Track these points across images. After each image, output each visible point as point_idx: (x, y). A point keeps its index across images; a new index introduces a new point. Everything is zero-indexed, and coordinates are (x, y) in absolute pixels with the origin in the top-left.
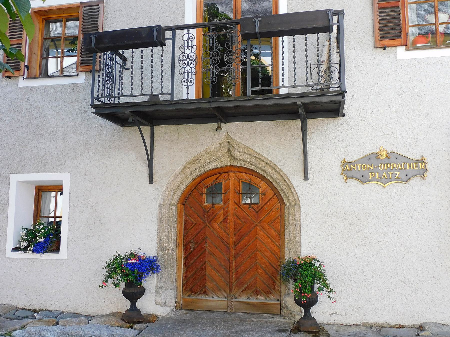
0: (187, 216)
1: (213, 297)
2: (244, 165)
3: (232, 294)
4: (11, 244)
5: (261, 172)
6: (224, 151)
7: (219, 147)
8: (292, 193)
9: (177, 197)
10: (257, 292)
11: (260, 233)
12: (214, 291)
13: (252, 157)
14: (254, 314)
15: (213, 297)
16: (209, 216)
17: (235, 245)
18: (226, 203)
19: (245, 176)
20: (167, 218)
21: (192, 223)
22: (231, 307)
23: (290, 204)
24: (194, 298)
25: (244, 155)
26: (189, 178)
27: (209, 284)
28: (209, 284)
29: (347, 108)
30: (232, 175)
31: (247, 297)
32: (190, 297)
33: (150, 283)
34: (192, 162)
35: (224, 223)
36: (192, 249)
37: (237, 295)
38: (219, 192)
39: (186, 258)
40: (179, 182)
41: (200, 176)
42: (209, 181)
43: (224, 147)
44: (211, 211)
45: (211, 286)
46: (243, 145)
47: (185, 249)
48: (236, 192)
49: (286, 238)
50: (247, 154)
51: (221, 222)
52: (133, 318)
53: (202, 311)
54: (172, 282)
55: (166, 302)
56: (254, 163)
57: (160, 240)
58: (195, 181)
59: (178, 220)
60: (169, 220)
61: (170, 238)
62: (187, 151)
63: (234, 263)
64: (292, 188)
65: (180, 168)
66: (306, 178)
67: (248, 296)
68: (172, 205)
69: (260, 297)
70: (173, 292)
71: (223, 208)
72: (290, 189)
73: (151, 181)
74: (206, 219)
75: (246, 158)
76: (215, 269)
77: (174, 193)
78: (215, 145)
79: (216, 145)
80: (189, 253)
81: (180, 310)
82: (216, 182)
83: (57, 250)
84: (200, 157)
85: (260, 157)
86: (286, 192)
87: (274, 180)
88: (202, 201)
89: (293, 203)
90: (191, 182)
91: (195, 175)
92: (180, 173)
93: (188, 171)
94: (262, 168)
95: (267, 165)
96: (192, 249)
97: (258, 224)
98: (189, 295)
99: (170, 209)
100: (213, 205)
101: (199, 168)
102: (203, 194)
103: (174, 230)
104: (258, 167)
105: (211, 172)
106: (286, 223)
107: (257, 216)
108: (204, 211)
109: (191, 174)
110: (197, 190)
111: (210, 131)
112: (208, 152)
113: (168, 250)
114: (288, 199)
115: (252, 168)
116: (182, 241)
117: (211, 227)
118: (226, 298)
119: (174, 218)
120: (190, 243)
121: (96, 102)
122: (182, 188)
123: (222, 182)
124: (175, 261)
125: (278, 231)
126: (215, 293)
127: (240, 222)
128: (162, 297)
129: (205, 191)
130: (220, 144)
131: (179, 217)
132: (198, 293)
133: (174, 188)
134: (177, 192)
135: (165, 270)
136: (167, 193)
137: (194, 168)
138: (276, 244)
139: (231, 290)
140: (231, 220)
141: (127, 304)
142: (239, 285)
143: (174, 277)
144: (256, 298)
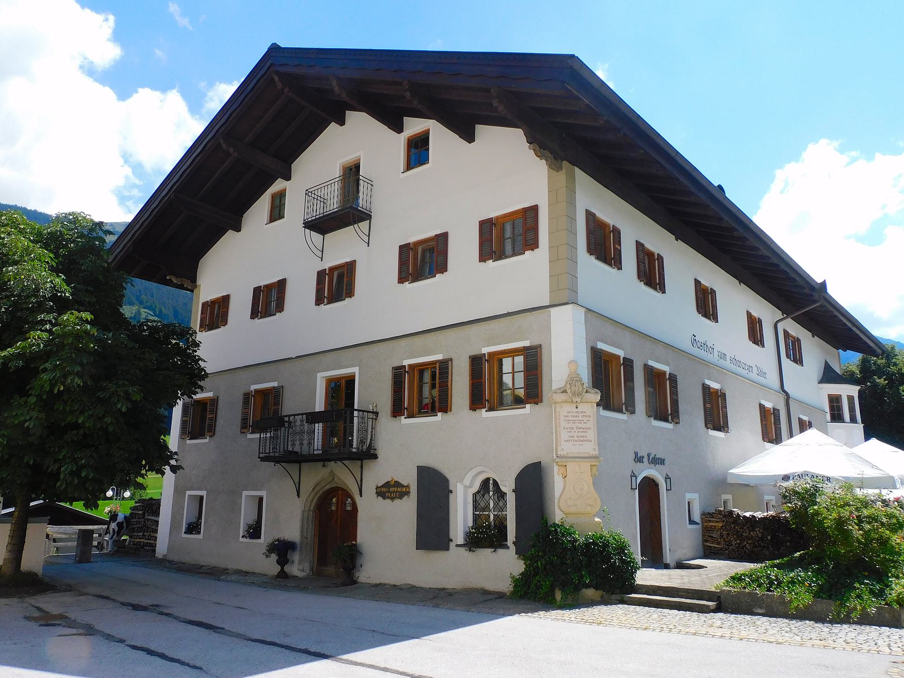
4: (241, 535)
29: (380, 453)
33: (296, 557)
52: (283, 575)
57: (302, 532)
62: (314, 478)
66: (361, 495)
73: (298, 496)
83: (259, 538)
93: (316, 490)
121: (261, 455)
141: (279, 568)
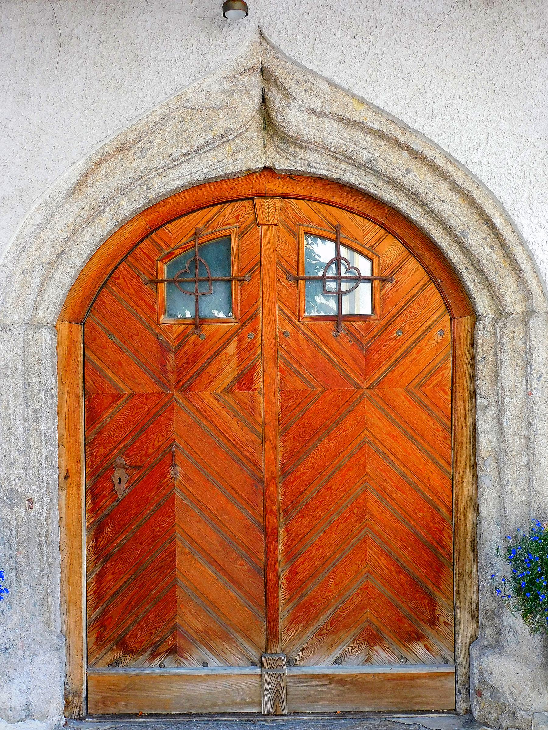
0: (96, 370)
1: (205, 665)
2: (324, 167)
3: (278, 649)
5: (388, 195)
6: (250, 106)
7: (228, 93)
8: (518, 272)
9: (56, 294)
10: (371, 638)
11: (378, 423)
12: (207, 640)
13: (359, 134)
14: (363, 715)
15: (205, 665)
16: (186, 361)
17: (286, 471)
18: (248, 318)
19: (317, 212)
20: (18, 378)
21: (117, 397)
22: (277, 695)
23: (501, 313)
24: (133, 671)
25: (328, 124)
26: (104, 218)
27: (189, 618)
28: (189, 617)
30: (270, 210)
31: (332, 658)
32: (119, 670)
34: (117, 151)
35: (240, 389)
36: (122, 491)
37: (296, 653)
38: (218, 274)
39: (98, 529)
40: (64, 235)
41: (145, 212)
42: (179, 232)
43: (248, 92)
44: (189, 346)
45: (197, 624)
46: (323, 85)
47: (95, 494)
48: (287, 272)
49: (487, 438)
50: (342, 120)
51: (229, 388)
53: (165, 716)
54: (48, 623)
55: (29, 703)
56: (364, 156)
58: (126, 234)
59: (62, 382)
60: (27, 386)
61: (34, 455)
63: (282, 536)
64: (519, 253)
65: (69, 176)
67: (337, 653)
68: (39, 326)
69: (380, 653)
70: (56, 661)
71: (237, 332)
72: (512, 260)
74: (172, 377)
75: (335, 135)
76: (214, 562)
77: (46, 279)
78: (209, 81)
79: (214, 84)
80: (107, 506)
81: (81, 719)
82: (207, 235)
84: (150, 131)
85: (394, 131)
86: (490, 267)
87: (441, 221)
88: (154, 310)
89: (518, 309)
90: (110, 236)
91: (128, 206)
92: (68, 196)
93: (100, 188)
94: (397, 175)
95: (416, 165)
96: (122, 491)
97: (368, 392)
98: (115, 663)
99: (28, 343)
100: (198, 322)
101: (140, 181)
102: (154, 282)
103: (50, 425)
104: (377, 173)
105: (187, 197)
106: (484, 384)
107: (367, 360)
108: (164, 348)
109: (111, 201)
110: (133, 267)
111: (190, 23)
112: (182, 109)
113: (30, 500)
114: (494, 295)
115: (352, 177)
116: (78, 461)
117: (190, 408)
118: (253, 664)
119: (47, 378)
120: (112, 468)
122: (78, 258)
123: (229, 236)
124: (58, 539)
125: (445, 415)
126: (213, 651)
127: (300, 386)
128: (14, 688)
129: (164, 270)
130: (231, 78)
131: (63, 371)
132: (148, 653)
133: (44, 259)
134: (58, 276)
135: (19, 580)
136: (18, 277)
137: (121, 178)
138: (437, 464)
139: (272, 635)
140: (268, 376)
142: (303, 615)
143: (55, 603)
144: (368, 660)
